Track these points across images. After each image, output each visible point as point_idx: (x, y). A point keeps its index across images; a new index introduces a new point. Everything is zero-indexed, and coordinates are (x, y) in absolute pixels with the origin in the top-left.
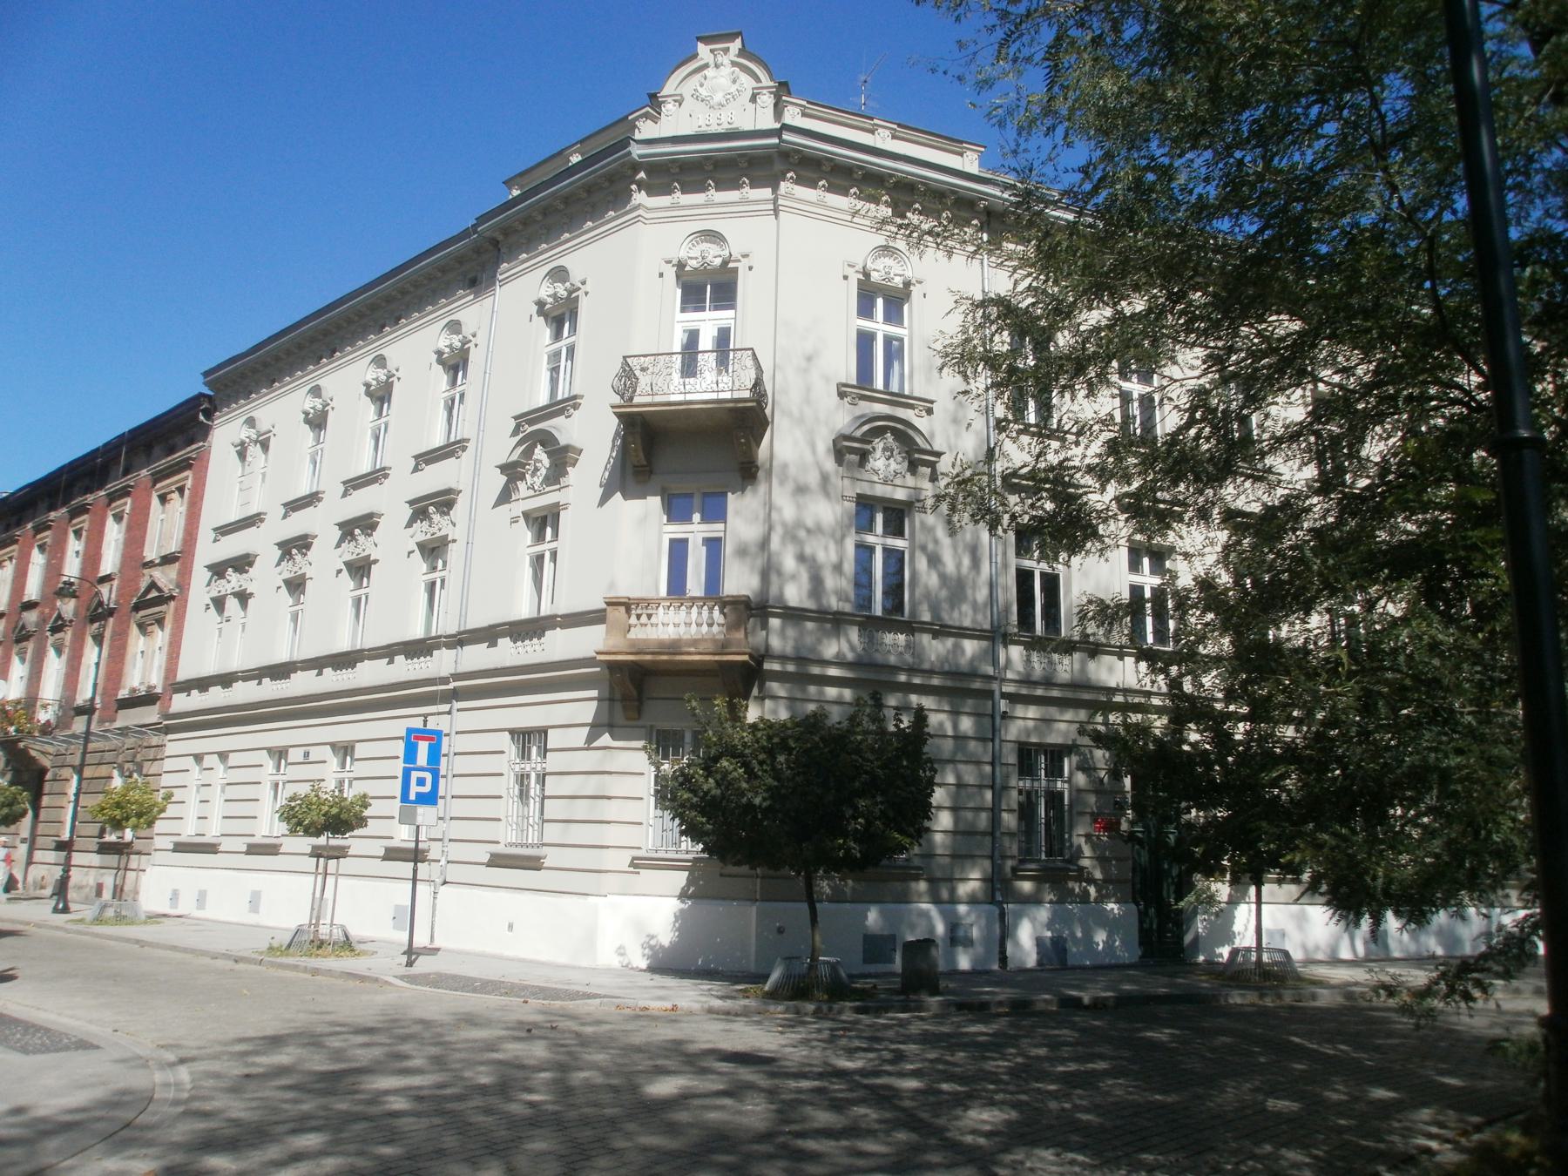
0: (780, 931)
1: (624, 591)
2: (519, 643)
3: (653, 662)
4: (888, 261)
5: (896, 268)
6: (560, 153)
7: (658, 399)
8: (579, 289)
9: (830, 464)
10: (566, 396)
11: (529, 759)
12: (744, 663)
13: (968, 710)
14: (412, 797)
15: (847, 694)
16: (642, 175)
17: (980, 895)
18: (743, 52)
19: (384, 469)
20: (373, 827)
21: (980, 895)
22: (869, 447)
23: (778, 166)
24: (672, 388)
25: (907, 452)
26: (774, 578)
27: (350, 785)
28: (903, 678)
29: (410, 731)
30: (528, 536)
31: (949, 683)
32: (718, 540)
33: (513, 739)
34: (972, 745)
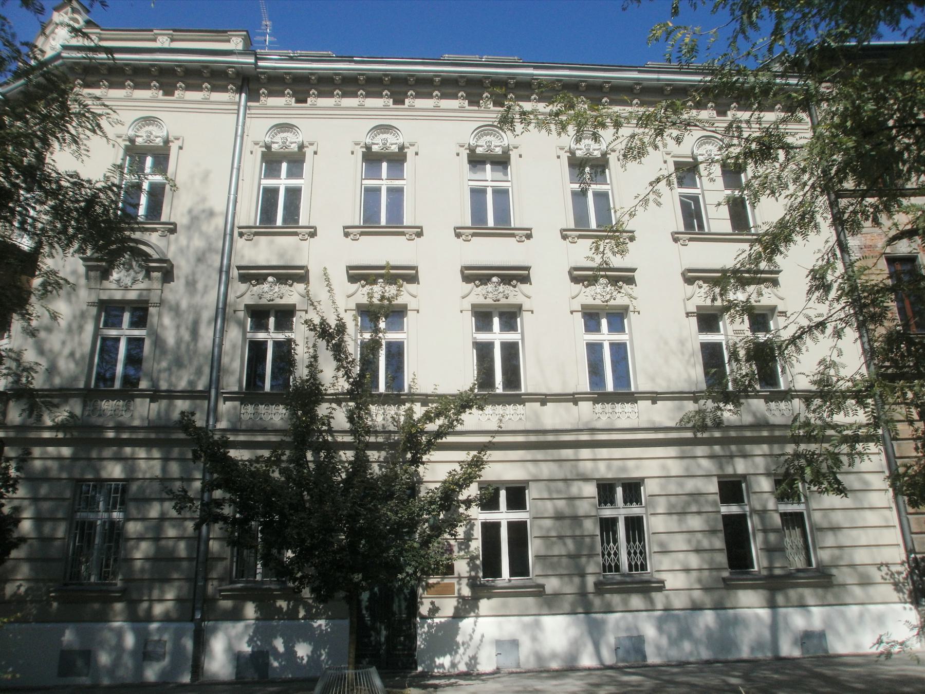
5: (495, 141)
15: (66, 451)
17: (174, 615)
21: (174, 615)
28: (111, 435)
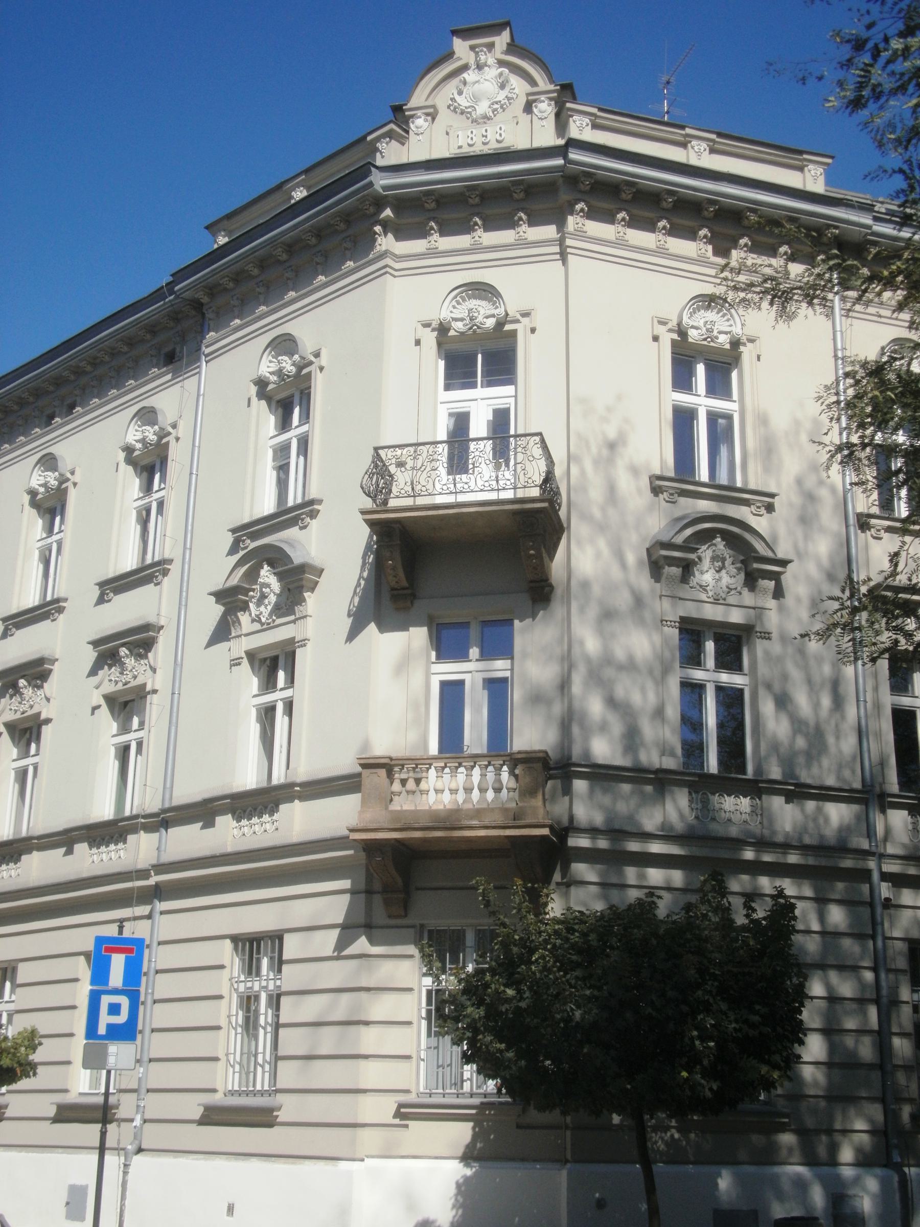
0: (601, 1204)
1: (381, 748)
2: (244, 822)
3: (424, 840)
4: (711, 315)
6: (279, 187)
7: (420, 501)
8: (311, 363)
9: (644, 582)
10: (299, 501)
11: (258, 974)
12: (543, 838)
13: (837, 897)
14: (102, 1030)
15: (677, 877)
16: (388, 212)
18: (513, 48)
19: (57, 601)
20: (44, 1077)
22: (693, 556)
23: (564, 196)
24: (438, 486)
25: (742, 562)
26: (576, 730)
27: (10, 1021)
28: (749, 854)
29: (99, 940)
30: (254, 683)
31: (811, 861)
32: (504, 680)
33: (236, 949)
34: (847, 943)
